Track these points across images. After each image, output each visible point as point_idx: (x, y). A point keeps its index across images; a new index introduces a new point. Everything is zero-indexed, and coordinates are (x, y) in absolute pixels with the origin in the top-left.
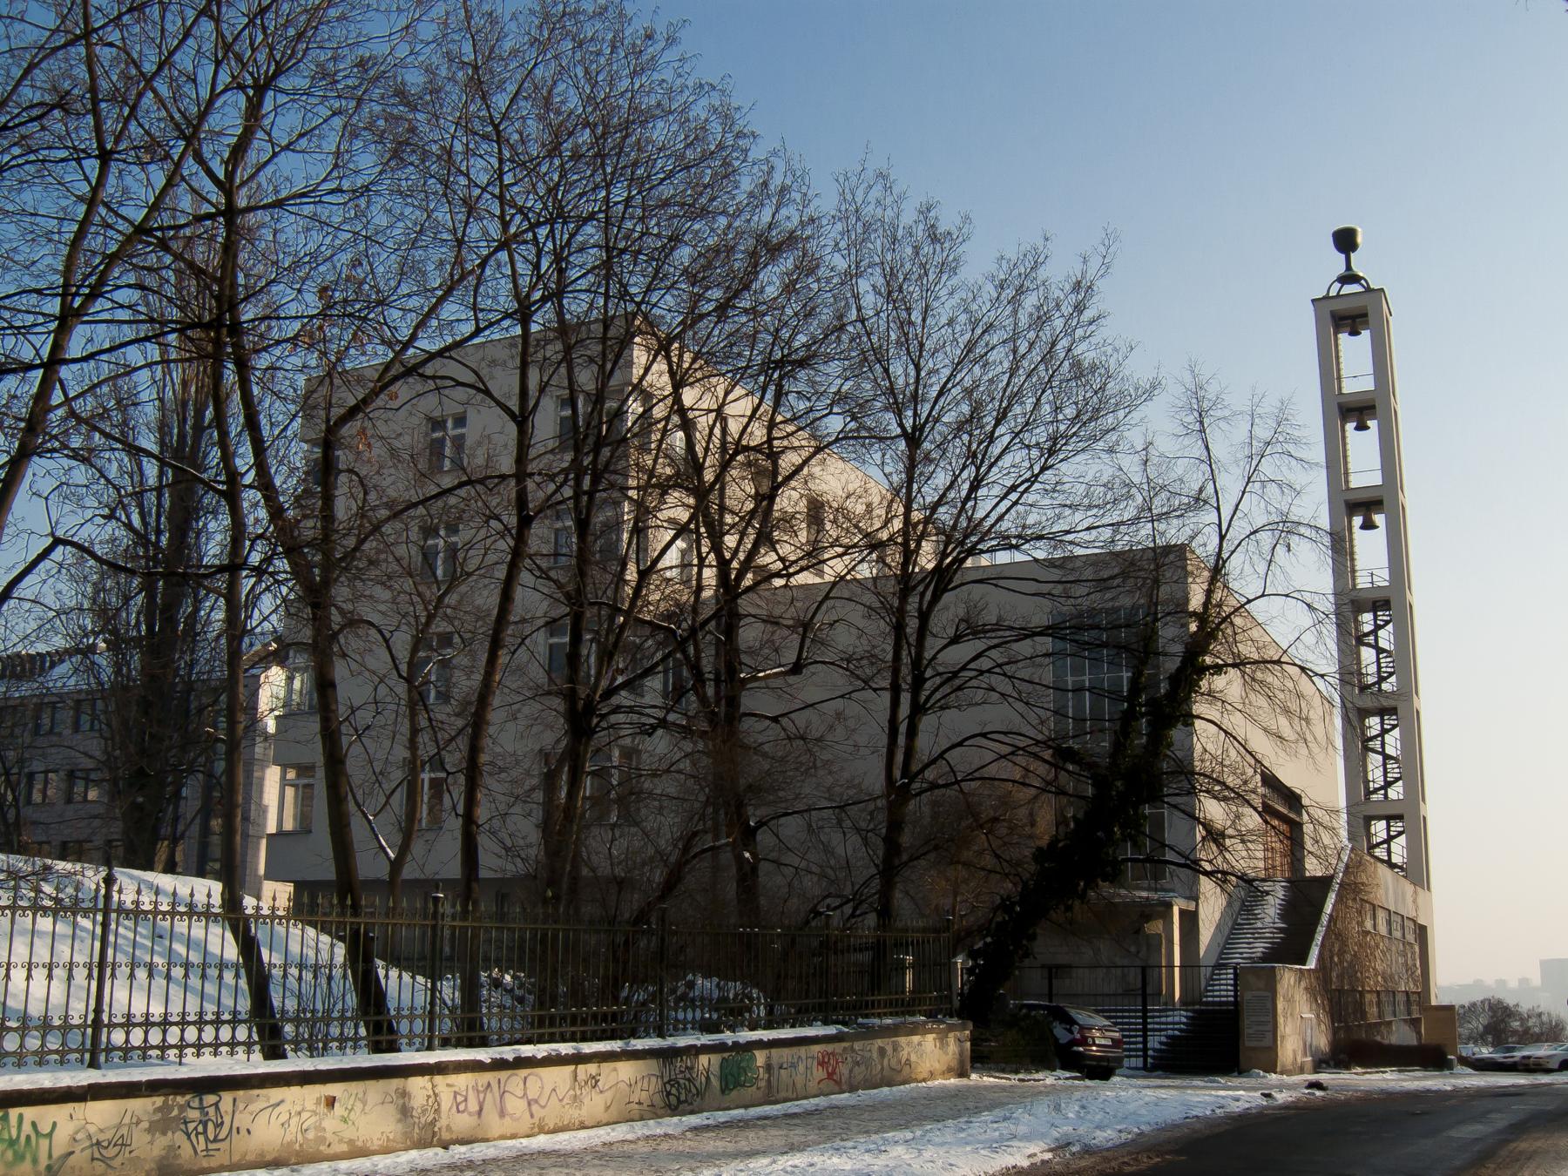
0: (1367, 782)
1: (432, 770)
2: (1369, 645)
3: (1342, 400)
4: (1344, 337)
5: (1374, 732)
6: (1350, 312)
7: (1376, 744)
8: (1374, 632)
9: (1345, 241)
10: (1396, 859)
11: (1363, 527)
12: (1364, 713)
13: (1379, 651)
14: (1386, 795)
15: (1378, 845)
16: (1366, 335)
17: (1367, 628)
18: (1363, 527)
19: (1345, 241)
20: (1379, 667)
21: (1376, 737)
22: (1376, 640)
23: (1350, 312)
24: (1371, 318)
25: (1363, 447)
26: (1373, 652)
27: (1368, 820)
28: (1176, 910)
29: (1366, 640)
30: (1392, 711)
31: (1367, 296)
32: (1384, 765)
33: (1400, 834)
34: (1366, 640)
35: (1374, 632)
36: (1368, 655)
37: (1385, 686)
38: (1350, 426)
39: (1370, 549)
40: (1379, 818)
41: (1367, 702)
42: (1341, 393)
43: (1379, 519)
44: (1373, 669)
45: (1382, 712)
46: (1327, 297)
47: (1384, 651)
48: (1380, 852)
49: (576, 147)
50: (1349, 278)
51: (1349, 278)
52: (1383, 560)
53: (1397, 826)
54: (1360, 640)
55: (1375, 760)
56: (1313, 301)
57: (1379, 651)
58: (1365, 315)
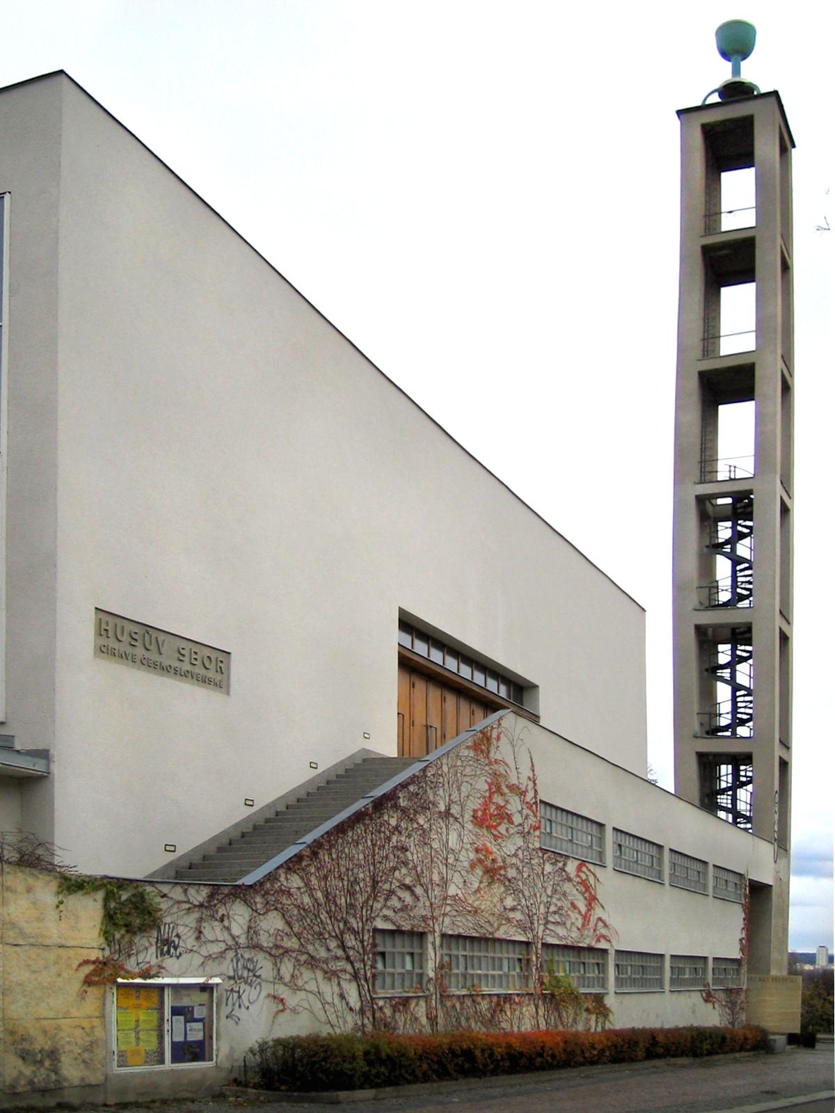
2: (722, 679)
8: (731, 665)
9: (736, 41)
13: (736, 688)
14: (734, 733)
15: (723, 791)
19: (736, 41)
22: (733, 549)
29: (720, 673)
35: (731, 665)
36: (723, 566)
47: (742, 687)
50: (736, 91)
53: (742, 650)
55: (723, 566)
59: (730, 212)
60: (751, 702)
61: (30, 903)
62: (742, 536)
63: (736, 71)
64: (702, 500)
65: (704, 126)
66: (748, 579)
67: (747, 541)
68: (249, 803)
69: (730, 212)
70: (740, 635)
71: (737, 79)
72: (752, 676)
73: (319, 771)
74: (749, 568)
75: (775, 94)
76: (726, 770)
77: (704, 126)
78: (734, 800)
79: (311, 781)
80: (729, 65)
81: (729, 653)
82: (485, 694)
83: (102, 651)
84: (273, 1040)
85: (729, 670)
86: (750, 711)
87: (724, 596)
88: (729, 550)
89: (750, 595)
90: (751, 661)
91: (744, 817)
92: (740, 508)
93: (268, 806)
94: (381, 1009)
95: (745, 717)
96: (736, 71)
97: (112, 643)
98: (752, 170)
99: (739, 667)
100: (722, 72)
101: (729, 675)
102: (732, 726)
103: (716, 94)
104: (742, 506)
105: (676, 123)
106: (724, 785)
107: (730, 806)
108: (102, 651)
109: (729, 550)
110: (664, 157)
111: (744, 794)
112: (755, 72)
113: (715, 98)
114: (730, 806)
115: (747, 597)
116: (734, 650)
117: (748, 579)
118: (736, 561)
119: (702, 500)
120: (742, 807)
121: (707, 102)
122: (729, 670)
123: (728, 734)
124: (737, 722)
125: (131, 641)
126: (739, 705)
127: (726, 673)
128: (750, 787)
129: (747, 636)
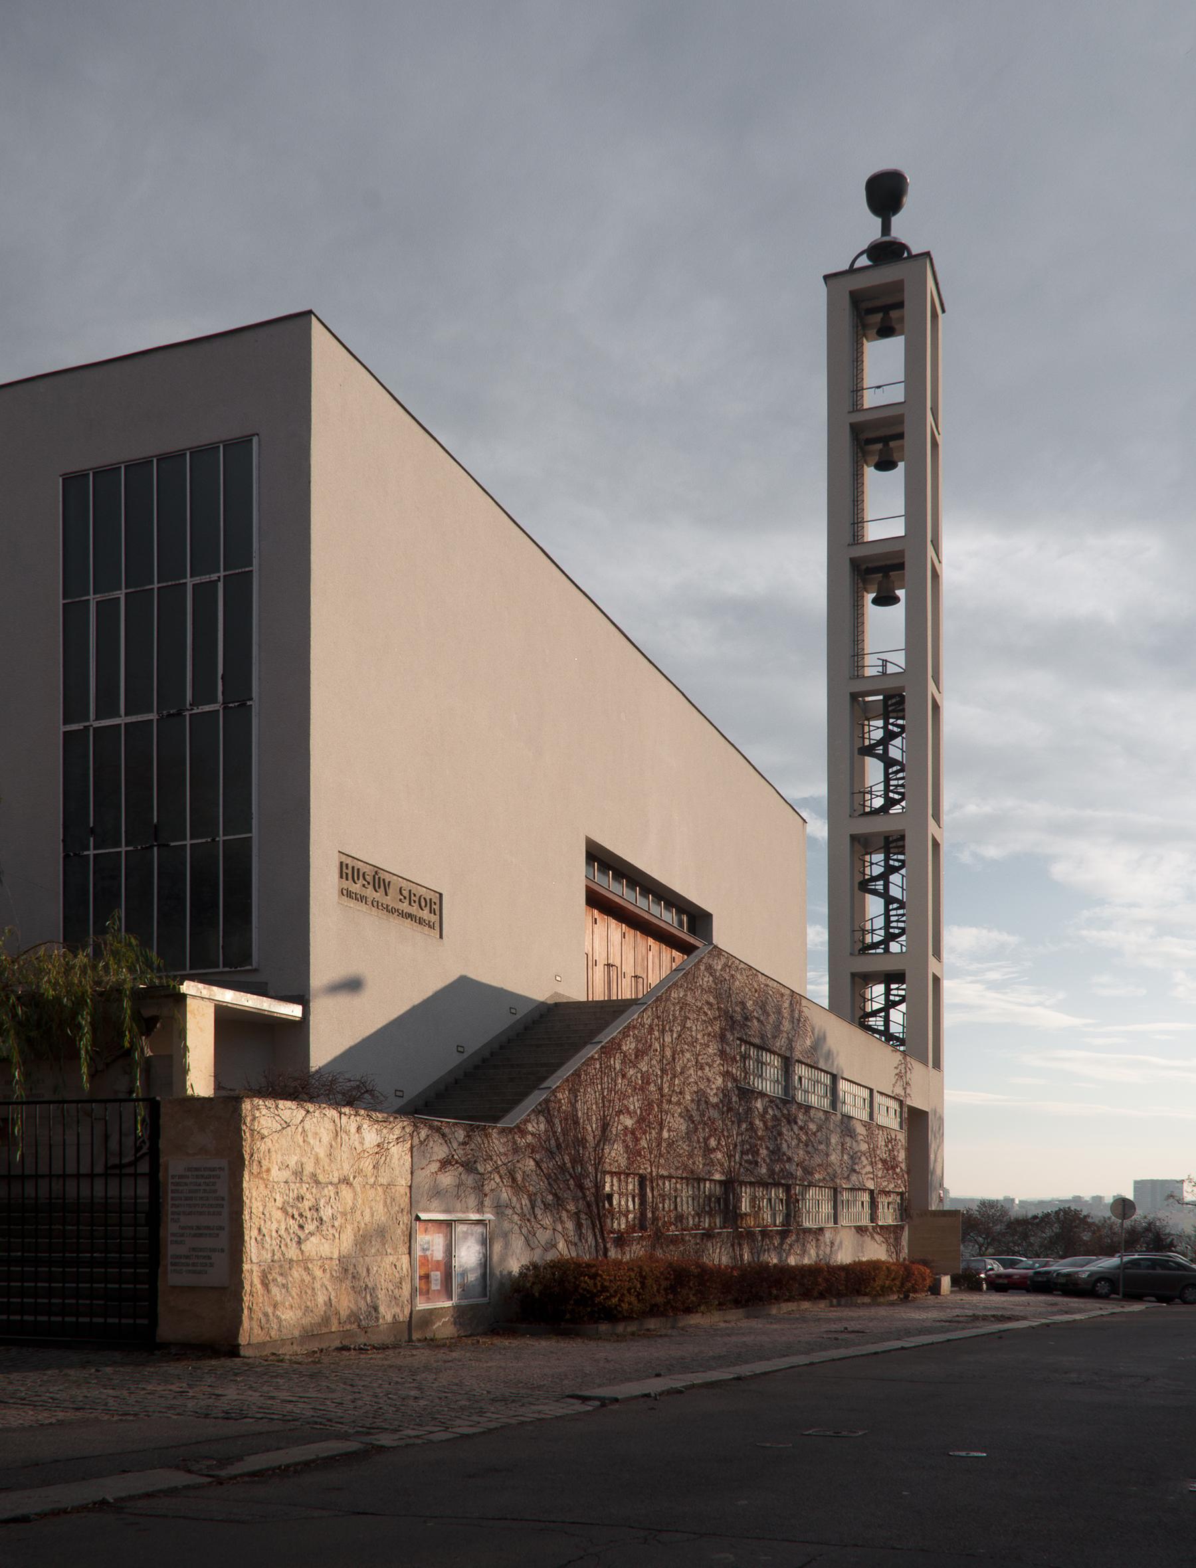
2: (875, 892)
4: (870, 473)
6: (879, 297)
8: (884, 877)
9: (886, 193)
12: (867, 979)
13: (889, 900)
14: (887, 950)
15: (874, 1013)
16: (899, 473)
18: (877, 602)
19: (886, 193)
20: (888, 921)
22: (886, 750)
23: (879, 297)
25: (885, 628)
26: (880, 765)
28: (97, 724)
29: (872, 1021)
30: (899, 977)
33: (903, 999)
34: (872, 1021)
35: (884, 877)
36: (874, 906)
37: (894, 947)
39: (885, 628)
41: (874, 963)
44: (880, 922)
45: (891, 978)
46: (852, 270)
47: (895, 900)
48: (877, 1022)
50: (886, 252)
51: (886, 252)
53: (897, 990)
54: (865, 886)
56: (826, 278)
57: (889, 900)
58: (901, 566)
59: (879, 387)
60: (903, 915)
62: (894, 736)
63: (886, 228)
64: (854, 697)
65: (853, 294)
66: (901, 782)
67: (898, 742)
68: (460, 1050)
69: (879, 387)
70: (893, 844)
71: (886, 239)
73: (518, 1017)
74: (902, 770)
75: (928, 254)
76: (879, 989)
77: (853, 294)
79: (511, 1027)
80: (879, 220)
81: (882, 863)
82: (646, 916)
83: (73, 482)
85: (881, 882)
86: (903, 993)
87: (878, 802)
89: (903, 731)
90: (903, 871)
91: (897, 1039)
93: (475, 1053)
95: (897, 931)
96: (886, 228)
97: (356, 888)
98: (903, 337)
100: (869, 229)
102: (886, 942)
103: (865, 256)
104: (894, 703)
105: (823, 289)
106: (876, 1006)
108: (73, 482)
110: (809, 315)
111: (897, 1015)
112: (903, 227)
113: (864, 261)
115: (898, 802)
116: (887, 859)
117: (901, 782)
118: (889, 763)
119: (854, 697)
120: (895, 1029)
121: (856, 265)
122: (881, 882)
124: (890, 937)
125: (366, 882)
126: (893, 919)
127: (880, 886)
128: (903, 1007)
129: (900, 843)
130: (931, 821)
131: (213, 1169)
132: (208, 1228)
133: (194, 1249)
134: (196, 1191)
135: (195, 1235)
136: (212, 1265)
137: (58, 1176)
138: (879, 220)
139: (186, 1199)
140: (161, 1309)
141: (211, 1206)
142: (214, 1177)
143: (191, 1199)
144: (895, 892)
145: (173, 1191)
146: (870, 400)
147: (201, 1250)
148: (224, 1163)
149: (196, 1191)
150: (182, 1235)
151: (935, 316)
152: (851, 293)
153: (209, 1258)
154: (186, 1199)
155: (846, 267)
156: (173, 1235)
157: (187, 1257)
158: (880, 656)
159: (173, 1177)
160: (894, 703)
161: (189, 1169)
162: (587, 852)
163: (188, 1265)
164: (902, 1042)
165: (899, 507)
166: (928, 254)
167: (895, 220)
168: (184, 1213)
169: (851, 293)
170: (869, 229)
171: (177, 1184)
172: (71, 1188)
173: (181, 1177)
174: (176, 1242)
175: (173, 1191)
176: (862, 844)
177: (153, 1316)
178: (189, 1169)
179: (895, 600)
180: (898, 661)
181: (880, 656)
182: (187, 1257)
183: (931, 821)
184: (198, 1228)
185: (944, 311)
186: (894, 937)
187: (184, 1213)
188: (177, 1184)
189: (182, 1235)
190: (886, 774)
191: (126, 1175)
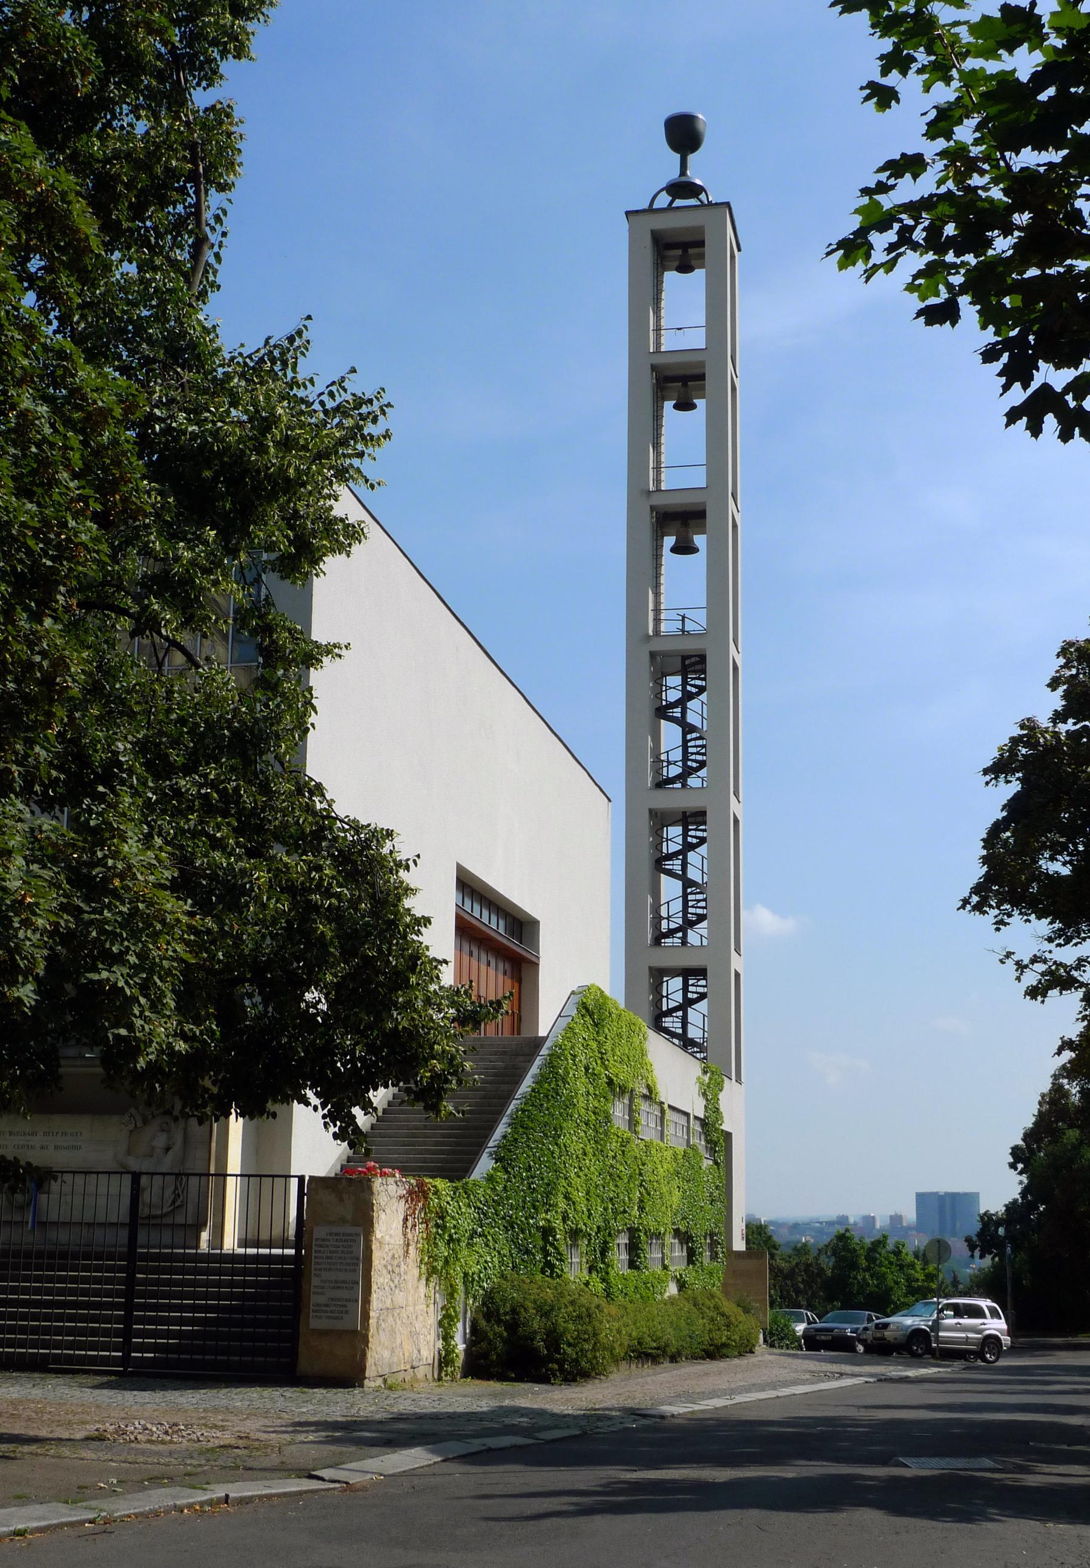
0: (657, 918)
1: (209, 827)
2: (670, 873)
3: (657, 646)
5: (674, 848)
7: (676, 865)
8: (682, 703)
9: (683, 134)
10: (694, 1033)
11: (675, 550)
14: (684, 942)
15: (670, 1012)
17: (674, 695)
18: (675, 550)
19: (683, 134)
21: (675, 855)
22: (684, 713)
24: (709, 249)
27: (659, 975)
29: (668, 865)
30: (701, 973)
31: (702, 212)
32: (685, 896)
35: (682, 703)
36: (670, 888)
38: (668, 405)
40: (673, 972)
41: (671, 953)
42: (658, 351)
43: (700, 540)
44: (677, 906)
46: (650, 210)
49: (147, 907)
50: (682, 188)
51: (682, 188)
52: (700, 598)
54: (659, 863)
55: (670, 888)
58: (702, 377)
61: (7, 205)
71: (683, 179)
72: (705, 870)
78: (684, 865)
84: (220, 114)
87: (675, 771)
88: (679, 715)
92: (692, 760)
94: (277, 457)
99: (689, 704)
100: (668, 166)
101: (680, 868)
102: (682, 777)
104: (693, 664)
107: (680, 1031)
109: (679, 715)
113: (663, 200)
114: (680, 1031)
122: (679, 710)
123: (679, 785)
124: (689, 924)
126: (691, 750)
130: (732, 797)
131: (351, 1235)
132: (344, 1282)
133: (332, 1299)
134: (336, 1252)
135: (334, 1288)
136: (347, 1312)
137: (89, 1224)
138: (677, 157)
139: (328, 1258)
140: (302, 1348)
141: (348, 1264)
142: (352, 1240)
143: (330, 1258)
144: (693, 874)
145: (316, 1252)
146: (670, 342)
147: (338, 1300)
148: (359, 1230)
149: (336, 1252)
150: (323, 1288)
151: (733, 257)
152: (652, 231)
153: (345, 1306)
154: (328, 1258)
155: (646, 206)
156: (316, 1287)
157: (326, 1305)
158: (679, 612)
159: (317, 1240)
160: (693, 664)
161: (331, 1234)
162: (458, 880)
163: (326, 1312)
164: (702, 1048)
165: (700, 455)
166: (728, 205)
167: (692, 158)
168: (325, 1269)
169: (652, 231)
170: (668, 166)
171: (321, 1246)
172: (99, 1233)
173: (323, 1240)
174: (318, 1293)
175: (316, 1252)
176: (660, 820)
177: (294, 1353)
178: (331, 1234)
179: (693, 550)
180: (698, 621)
181: (679, 612)
182: (326, 1305)
183: (732, 797)
184: (336, 1282)
185: (739, 250)
186: (691, 924)
187: (325, 1269)
188: (321, 1246)
189: (323, 1288)
190: (685, 742)
191: (165, 1225)
